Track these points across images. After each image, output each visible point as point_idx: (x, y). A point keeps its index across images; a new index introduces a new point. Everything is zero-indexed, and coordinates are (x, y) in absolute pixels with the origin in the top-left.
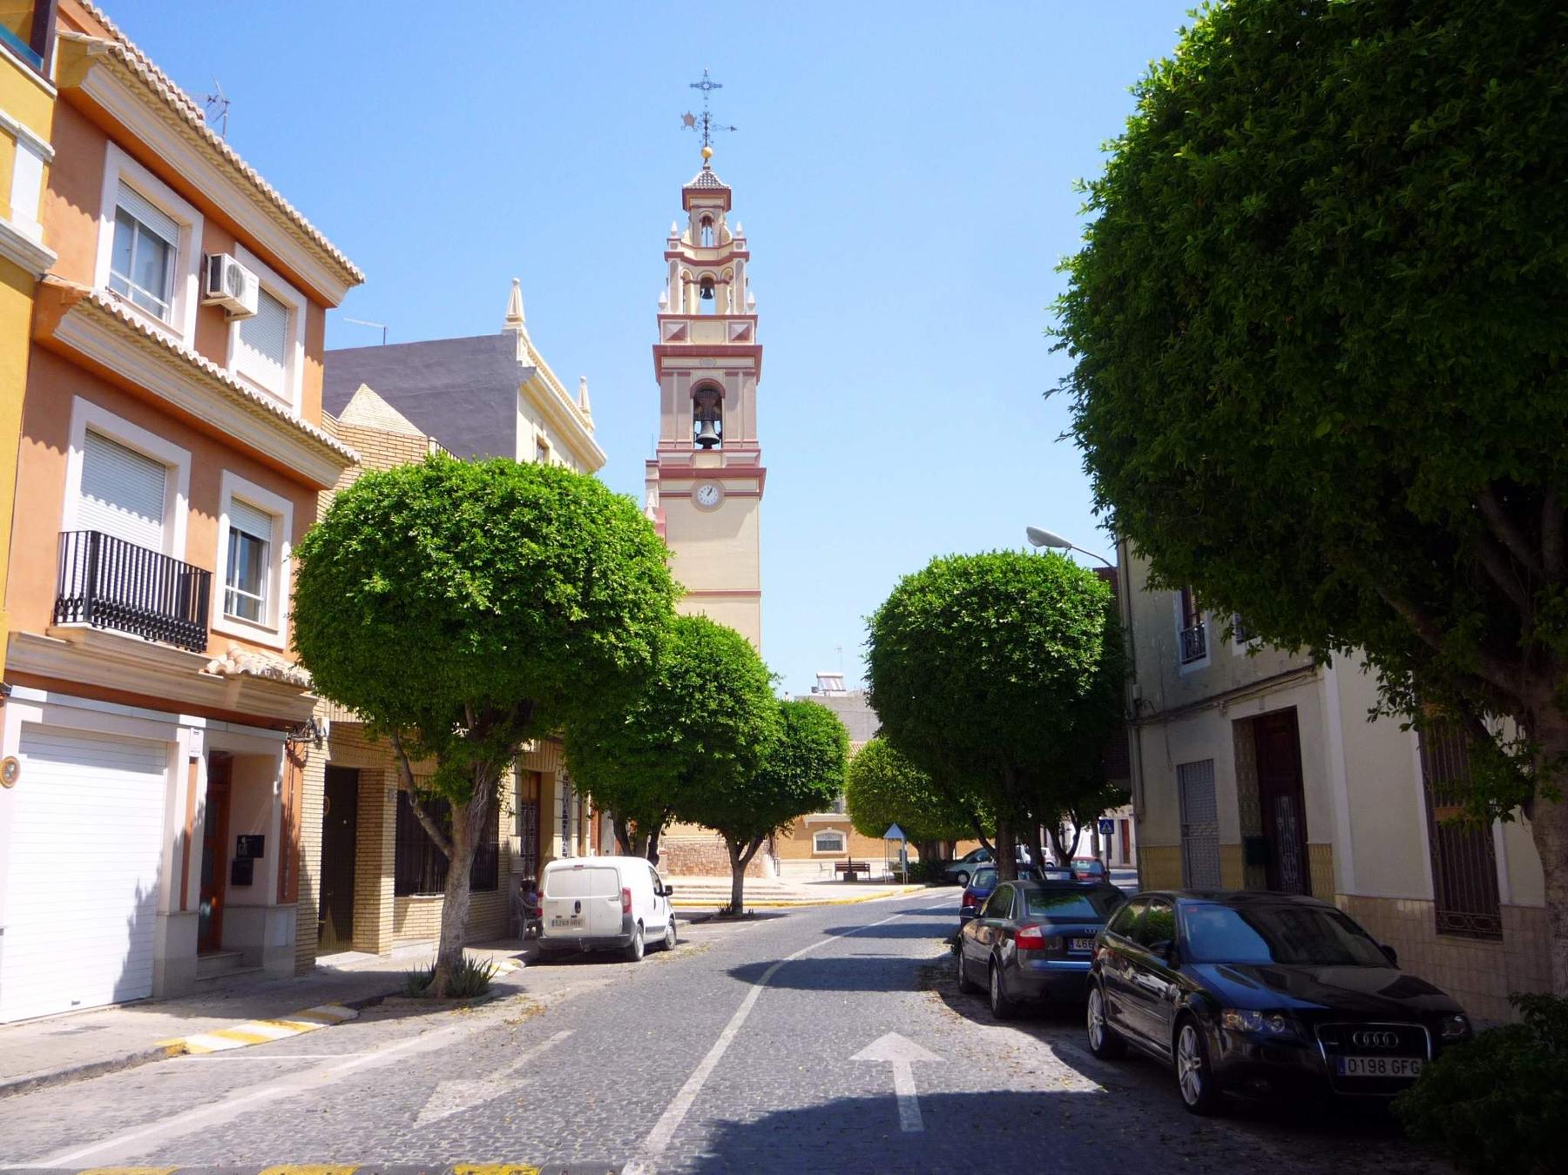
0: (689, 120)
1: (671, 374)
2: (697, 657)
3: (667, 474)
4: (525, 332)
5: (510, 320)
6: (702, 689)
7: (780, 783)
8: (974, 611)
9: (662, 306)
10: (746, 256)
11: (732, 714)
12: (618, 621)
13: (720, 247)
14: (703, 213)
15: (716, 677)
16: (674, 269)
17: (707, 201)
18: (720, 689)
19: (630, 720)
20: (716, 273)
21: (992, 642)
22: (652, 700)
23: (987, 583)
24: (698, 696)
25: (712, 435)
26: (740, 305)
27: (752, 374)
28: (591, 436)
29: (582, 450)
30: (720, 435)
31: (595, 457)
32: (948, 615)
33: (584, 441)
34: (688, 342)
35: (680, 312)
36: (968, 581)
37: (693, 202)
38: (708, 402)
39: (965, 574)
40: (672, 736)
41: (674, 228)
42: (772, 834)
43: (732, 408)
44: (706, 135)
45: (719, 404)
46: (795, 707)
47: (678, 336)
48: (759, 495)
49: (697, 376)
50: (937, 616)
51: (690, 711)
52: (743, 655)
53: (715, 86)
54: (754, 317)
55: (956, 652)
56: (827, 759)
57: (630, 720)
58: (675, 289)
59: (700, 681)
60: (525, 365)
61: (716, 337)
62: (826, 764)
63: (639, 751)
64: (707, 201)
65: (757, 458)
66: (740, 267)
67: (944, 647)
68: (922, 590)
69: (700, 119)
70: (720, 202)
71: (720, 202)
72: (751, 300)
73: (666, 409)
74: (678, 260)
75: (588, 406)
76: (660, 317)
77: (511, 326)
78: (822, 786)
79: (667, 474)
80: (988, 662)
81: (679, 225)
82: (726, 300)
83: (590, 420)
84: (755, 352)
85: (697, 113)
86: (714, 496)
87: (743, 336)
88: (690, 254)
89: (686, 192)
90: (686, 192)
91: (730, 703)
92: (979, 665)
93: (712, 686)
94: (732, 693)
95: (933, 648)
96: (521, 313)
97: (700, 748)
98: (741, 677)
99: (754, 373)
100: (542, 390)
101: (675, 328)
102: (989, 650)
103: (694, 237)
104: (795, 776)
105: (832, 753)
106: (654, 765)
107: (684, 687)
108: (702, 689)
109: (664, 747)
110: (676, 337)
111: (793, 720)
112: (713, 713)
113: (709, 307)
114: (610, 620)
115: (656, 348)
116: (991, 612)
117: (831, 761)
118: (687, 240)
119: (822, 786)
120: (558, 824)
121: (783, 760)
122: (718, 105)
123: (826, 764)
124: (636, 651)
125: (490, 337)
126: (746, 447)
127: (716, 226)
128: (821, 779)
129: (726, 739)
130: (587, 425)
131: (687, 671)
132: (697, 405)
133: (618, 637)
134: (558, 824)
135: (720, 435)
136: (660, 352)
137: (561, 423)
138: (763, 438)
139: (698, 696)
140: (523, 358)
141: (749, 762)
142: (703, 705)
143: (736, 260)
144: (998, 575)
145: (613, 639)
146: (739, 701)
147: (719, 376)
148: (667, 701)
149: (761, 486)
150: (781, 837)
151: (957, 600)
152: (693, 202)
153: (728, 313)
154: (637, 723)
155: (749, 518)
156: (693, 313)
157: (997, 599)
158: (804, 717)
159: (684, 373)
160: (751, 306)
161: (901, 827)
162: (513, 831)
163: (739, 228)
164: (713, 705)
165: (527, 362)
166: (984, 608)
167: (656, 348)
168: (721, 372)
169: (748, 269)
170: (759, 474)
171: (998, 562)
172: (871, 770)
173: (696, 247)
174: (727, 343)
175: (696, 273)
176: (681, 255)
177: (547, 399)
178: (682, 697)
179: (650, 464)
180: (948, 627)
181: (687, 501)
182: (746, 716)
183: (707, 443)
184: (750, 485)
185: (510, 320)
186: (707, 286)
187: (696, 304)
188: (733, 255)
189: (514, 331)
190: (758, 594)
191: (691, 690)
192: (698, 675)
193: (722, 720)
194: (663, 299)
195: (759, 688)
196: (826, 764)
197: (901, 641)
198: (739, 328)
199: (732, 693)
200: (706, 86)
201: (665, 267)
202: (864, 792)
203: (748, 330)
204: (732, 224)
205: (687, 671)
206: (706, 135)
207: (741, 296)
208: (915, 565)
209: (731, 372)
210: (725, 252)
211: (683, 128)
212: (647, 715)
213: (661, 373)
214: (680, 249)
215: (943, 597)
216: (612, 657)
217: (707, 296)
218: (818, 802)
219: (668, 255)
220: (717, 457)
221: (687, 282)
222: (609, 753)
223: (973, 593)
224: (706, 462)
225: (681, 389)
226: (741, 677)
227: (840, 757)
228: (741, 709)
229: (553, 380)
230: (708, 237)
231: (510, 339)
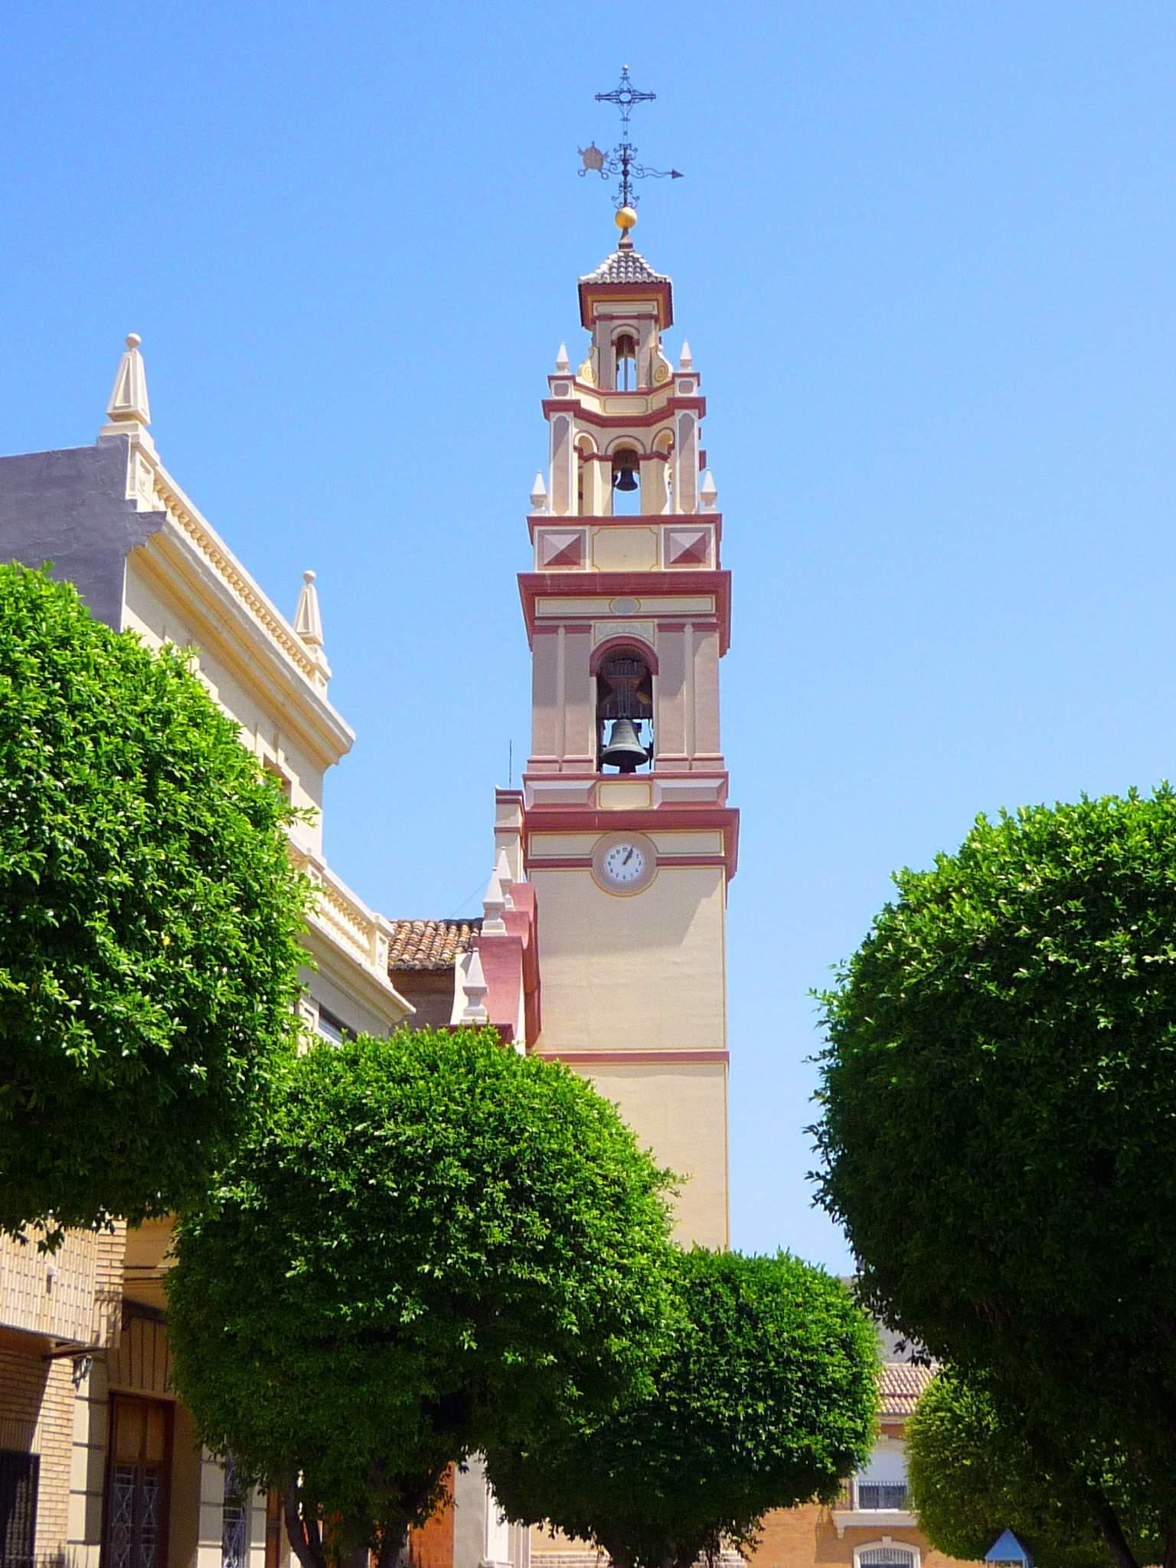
0: (594, 158)
1: (554, 630)
2: (465, 1121)
3: (538, 823)
4: (147, 441)
5: (117, 417)
6: (473, 1195)
7: (719, 1434)
8: (1073, 935)
9: (537, 501)
10: (699, 404)
11: (546, 1257)
12: (74, 943)
13: (650, 391)
14: (619, 328)
15: (509, 1168)
16: (561, 431)
17: (625, 307)
18: (518, 1197)
19: (299, 1266)
20: (642, 439)
21: (1124, 1016)
22: (353, 1220)
23: (1109, 863)
24: (461, 1211)
25: (630, 744)
26: (688, 497)
27: (711, 627)
28: (320, 691)
29: (293, 713)
30: (650, 751)
31: (327, 734)
32: (1004, 949)
33: (298, 694)
34: (588, 568)
35: (573, 511)
36: (1060, 863)
37: (599, 309)
38: (625, 683)
39: (1050, 846)
40: (399, 1308)
41: (563, 356)
42: (714, 1548)
43: (673, 692)
44: (625, 187)
45: (646, 687)
46: (756, 1267)
47: (566, 557)
48: (727, 864)
49: (603, 633)
50: (975, 954)
51: (444, 1247)
52: (579, 1122)
53: (643, 97)
54: (715, 519)
55: (1027, 1046)
56: (824, 1382)
57: (299, 1266)
58: (562, 470)
59: (467, 1178)
60: (143, 507)
61: (641, 556)
62: (826, 1395)
63: (327, 1344)
64: (625, 307)
65: (722, 790)
66: (687, 425)
67: (991, 1034)
68: (943, 898)
69: (613, 156)
70: (651, 308)
71: (651, 308)
72: (709, 487)
73: (543, 695)
74: (569, 416)
75: (317, 630)
76: (533, 522)
77: (115, 429)
78: (816, 1443)
79: (538, 823)
80: (1113, 1072)
81: (575, 355)
82: (665, 488)
83: (320, 657)
84: (717, 585)
85: (608, 145)
86: (635, 867)
87: (692, 555)
88: (590, 404)
89: (585, 289)
90: (585, 289)
91: (540, 1229)
92: (1091, 1080)
93: (497, 1190)
94: (547, 1207)
95: (968, 1040)
96: (141, 403)
97: (468, 1341)
98: (571, 1171)
99: (719, 624)
100: (188, 569)
101: (561, 542)
102: (1115, 1038)
103: (600, 374)
104: (753, 1419)
105: (837, 1369)
106: (356, 1378)
107: (429, 1192)
108: (473, 1195)
109: (381, 1335)
110: (562, 559)
111: (749, 1295)
112: (499, 1254)
113: (630, 503)
114: (47, 935)
115: (525, 580)
116: (1121, 937)
117: (836, 1387)
118: (586, 379)
119: (816, 1443)
120: (212, 1518)
121: (727, 1384)
122: (650, 133)
123: (826, 1395)
124: (128, 1025)
125: (70, 454)
126: (698, 768)
127: (642, 352)
128: (813, 1428)
129: (533, 1315)
130: (311, 669)
131: (439, 1153)
132: (604, 690)
133: (73, 986)
134: (212, 1518)
135: (650, 751)
136: (532, 588)
137: (235, 647)
138: (736, 751)
139: (461, 1211)
140: (142, 492)
141: (602, 1379)
142: (475, 1236)
143: (679, 414)
144: (1137, 838)
145: (53, 988)
146: (566, 1226)
147: (645, 632)
148: (387, 1223)
149: (731, 844)
150: (732, 1553)
151: (1030, 908)
152: (599, 309)
153: (666, 511)
154: (316, 1275)
155: (708, 907)
156: (598, 511)
157: (1137, 904)
158: (775, 1290)
159: (579, 626)
160: (709, 498)
161: (1022, 1539)
162: (77, 1527)
163: (686, 355)
164: (497, 1235)
165: (147, 501)
166: (1102, 929)
167: (525, 580)
168: (651, 624)
169: (706, 432)
170: (725, 822)
171: (1139, 817)
172: (956, 1419)
173: (603, 392)
174: (663, 569)
175: (607, 440)
176: (574, 407)
177: (201, 591)
178: (423, 1215)
179: (506, 798)
180: (1006, 982)
181: (582, 875)
182: (583, 1262)
183: (627, 761)
184: (711, 842)
185: (117, 417)
186: (625, 467)
187: (602, 498)
188: (675, 404)
189: (124, 439)
190: (723, 1057)
191: (445, 1198)
192: (466, 1164)
193: (521, 1271)
194: (539, 489)
195: (618, 1201)
196: (824, 1393)
197: (884, 1032)
198: (686, 540)
199: (547, 1207)
200: (626, 96)
201: (545, 428)
202: (944, 1463)
203: (703, 543)
204: (673, 350)
205: (439, 1153)
206: (625, 187)
207: (688, 481)
208: (930, 844)
209: (670, 625)
210: (658, 401)
211: (582, 173)
212: (340, 1257)
213: (537, 627)
214: (573, 395)
215: (993, 907)
216: (53, 1038)
217: (627, 484)
218: (811, 1479)
219: (549, 407)
220: (642, 788)
221: (585, 458)
222: (256, 1349)
223: (1067, 889)
224: (621, 797)
225: (574, 657)
226: (571, 1171)
227: (857, 1378)
228: (569, 1249)
229: (204, 539)
230: (631, 373)
231: (114, 456)
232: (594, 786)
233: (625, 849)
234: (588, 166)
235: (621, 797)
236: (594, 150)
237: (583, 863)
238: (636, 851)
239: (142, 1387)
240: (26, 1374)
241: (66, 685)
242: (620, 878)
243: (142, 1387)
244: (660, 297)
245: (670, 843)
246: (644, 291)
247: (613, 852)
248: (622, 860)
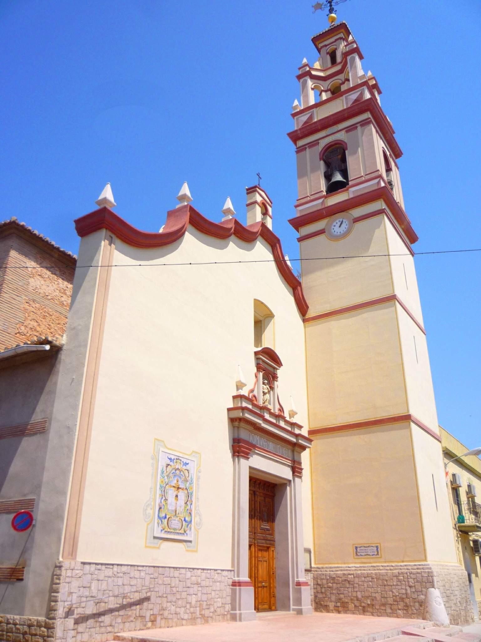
43: (355, 152)
49: (323, 143)
89: (315, 40)
147: (341, 136)
159: (315, 143)
168: (343, 132)
181: (322, 237)
225: (313, 156)
232: (323, 201)
233: (339, 221)
234: (316, 10)
235: (340, 198)
236: (318, 4)
237: (322, 232)
238: (344, 221)
239: (238, 576)
240: (355, 570)
241: (68, 577)
242: (339, 233)
243: (238, 576)
244: (343, 30)
245: (357, 212)
246: (337, 30)
247: (335, 224)
248: (338, 225)
